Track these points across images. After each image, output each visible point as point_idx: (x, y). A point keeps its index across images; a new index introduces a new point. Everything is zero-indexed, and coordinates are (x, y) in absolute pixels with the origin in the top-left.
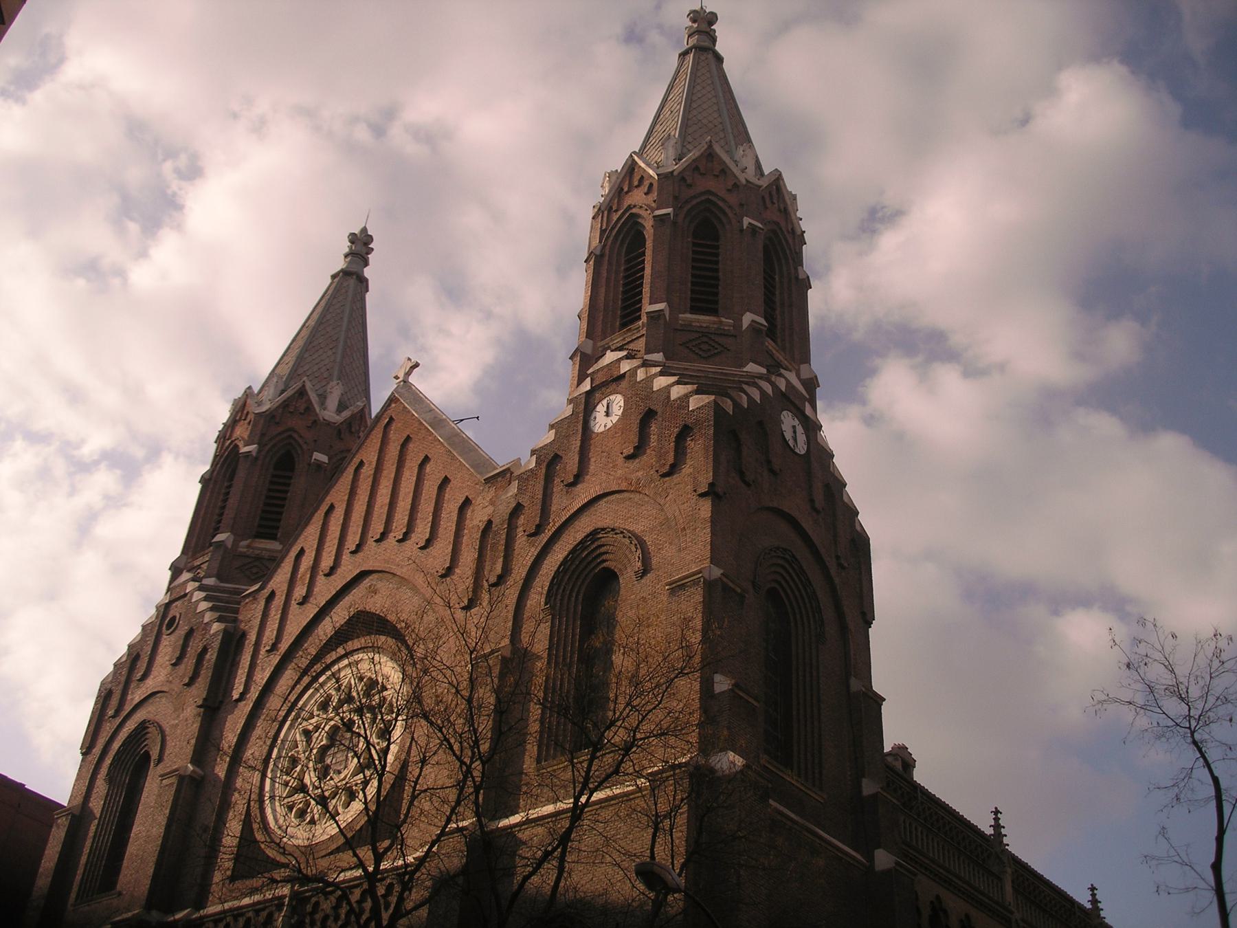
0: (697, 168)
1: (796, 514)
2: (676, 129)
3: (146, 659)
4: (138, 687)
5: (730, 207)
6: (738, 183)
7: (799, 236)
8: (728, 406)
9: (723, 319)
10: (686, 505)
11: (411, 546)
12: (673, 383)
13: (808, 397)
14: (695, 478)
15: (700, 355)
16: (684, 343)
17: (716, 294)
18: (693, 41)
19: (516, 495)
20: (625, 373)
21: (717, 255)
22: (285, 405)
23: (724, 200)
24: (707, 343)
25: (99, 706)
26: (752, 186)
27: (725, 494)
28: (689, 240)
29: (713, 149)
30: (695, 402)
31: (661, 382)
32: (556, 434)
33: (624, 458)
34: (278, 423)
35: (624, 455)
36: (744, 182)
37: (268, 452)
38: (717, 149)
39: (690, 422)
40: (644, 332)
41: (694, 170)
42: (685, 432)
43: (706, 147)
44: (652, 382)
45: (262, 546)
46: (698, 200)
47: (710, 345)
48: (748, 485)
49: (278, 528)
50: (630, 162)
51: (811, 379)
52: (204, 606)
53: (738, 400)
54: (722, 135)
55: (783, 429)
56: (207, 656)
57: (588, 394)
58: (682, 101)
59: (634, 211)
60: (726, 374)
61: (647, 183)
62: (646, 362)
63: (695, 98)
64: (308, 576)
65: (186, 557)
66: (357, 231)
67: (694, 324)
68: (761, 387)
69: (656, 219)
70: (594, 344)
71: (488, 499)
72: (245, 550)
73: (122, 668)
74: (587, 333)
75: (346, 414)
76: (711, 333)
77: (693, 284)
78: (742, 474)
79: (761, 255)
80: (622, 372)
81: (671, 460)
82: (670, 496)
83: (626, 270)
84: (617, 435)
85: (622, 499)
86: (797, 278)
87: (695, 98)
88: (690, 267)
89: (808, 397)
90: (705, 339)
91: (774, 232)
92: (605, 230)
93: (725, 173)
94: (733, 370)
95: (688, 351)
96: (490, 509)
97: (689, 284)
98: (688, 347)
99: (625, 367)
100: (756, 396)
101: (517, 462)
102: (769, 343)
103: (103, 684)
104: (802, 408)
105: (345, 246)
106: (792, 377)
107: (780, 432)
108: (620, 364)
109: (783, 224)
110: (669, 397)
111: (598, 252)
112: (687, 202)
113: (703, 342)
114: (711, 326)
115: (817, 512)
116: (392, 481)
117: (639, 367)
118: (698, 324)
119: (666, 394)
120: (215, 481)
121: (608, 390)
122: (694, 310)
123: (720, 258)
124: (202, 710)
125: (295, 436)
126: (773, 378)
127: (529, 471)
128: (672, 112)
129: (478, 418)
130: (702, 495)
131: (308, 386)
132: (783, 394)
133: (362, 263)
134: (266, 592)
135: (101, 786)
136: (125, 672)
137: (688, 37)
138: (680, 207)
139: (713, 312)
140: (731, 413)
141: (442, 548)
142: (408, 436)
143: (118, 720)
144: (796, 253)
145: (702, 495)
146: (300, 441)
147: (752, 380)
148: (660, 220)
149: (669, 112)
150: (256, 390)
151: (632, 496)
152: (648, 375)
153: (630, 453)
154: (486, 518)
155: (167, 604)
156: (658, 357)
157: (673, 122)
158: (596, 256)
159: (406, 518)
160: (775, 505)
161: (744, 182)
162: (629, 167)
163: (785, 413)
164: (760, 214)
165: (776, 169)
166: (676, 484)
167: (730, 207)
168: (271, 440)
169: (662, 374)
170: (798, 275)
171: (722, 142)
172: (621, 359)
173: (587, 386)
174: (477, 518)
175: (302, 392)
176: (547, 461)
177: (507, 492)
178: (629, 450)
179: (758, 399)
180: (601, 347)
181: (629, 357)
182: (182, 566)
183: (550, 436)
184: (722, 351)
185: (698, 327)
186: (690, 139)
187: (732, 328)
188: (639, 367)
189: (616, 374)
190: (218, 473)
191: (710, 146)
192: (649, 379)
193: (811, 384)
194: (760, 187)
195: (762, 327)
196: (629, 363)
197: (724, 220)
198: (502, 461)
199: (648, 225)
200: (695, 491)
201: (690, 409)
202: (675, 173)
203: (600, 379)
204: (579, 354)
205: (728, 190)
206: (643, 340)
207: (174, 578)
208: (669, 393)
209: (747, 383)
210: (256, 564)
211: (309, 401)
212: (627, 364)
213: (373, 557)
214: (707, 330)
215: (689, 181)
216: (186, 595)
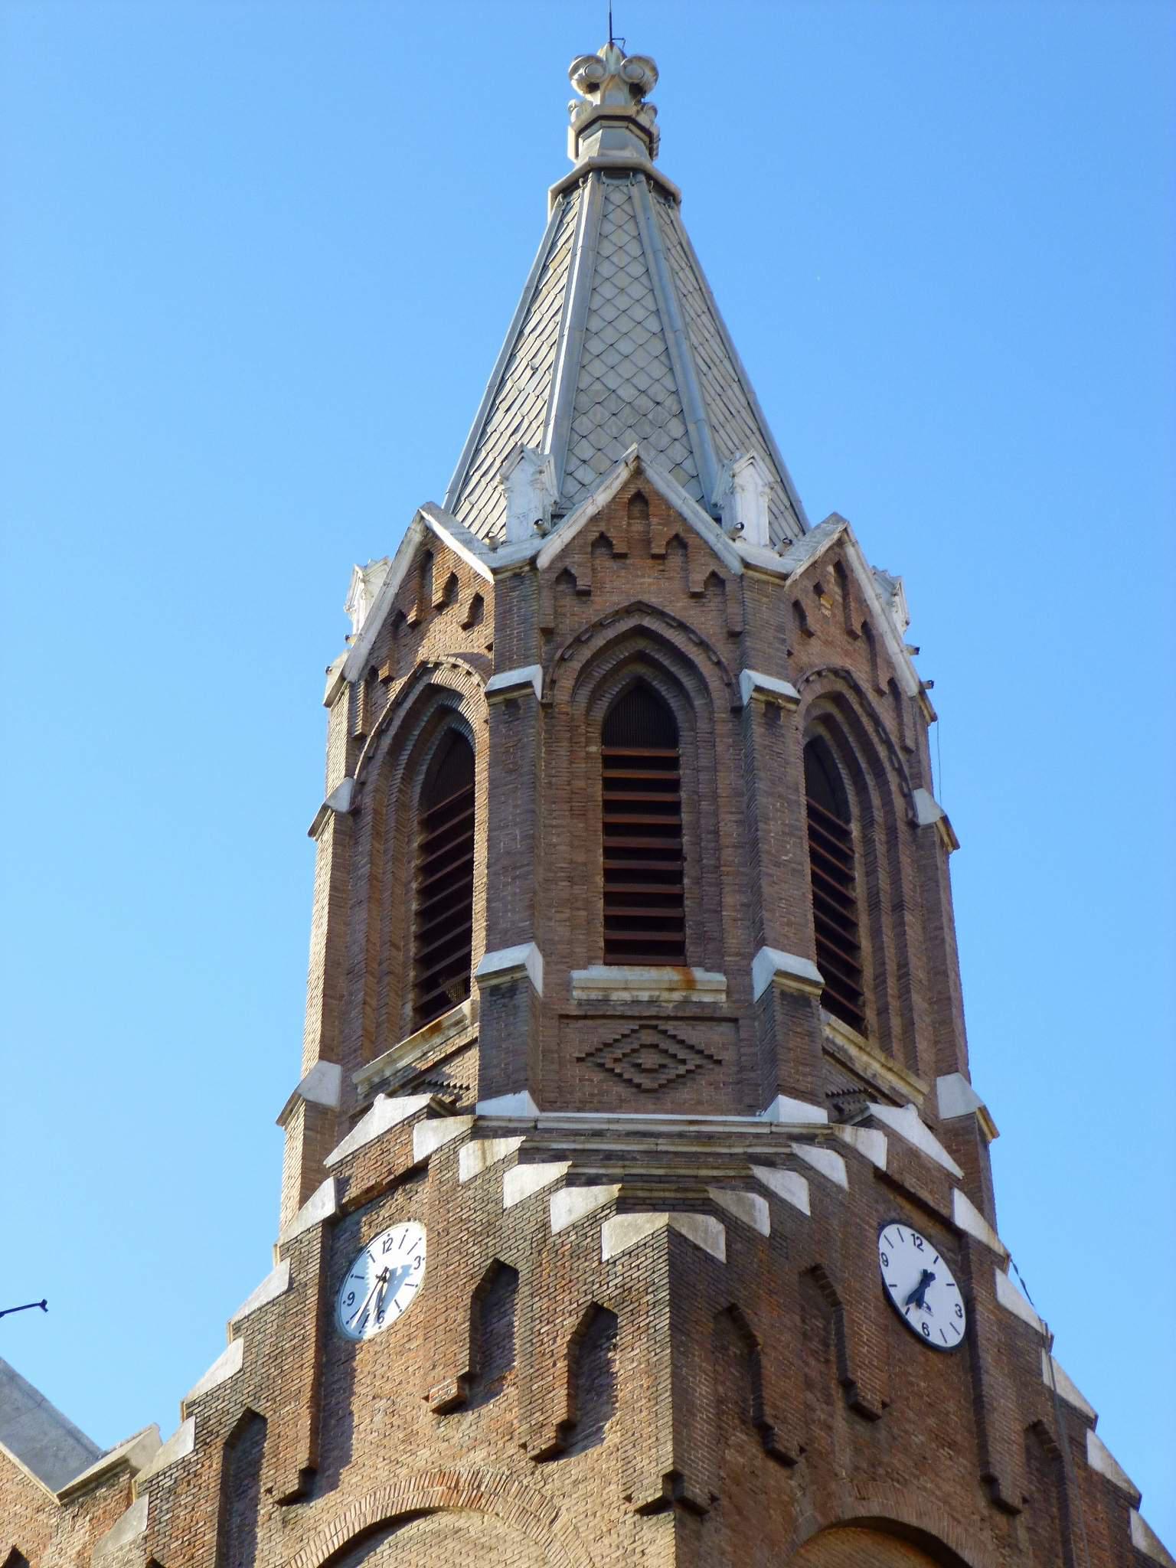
0: (603, 541)
1: (937, 1525)
2: (546, 423)
5: (702, 644)
6: (722, 574)
7: (912, 699)
9: (699, 974)
10: (606, 1541)
12: (558, 1181)
13: (958, 1172)
14: (627, 1461)
15: (638, 1086)
16: (589, 1055)
17: (678, 900)
18: (590, 148)
19: (145, 1538)
20: (428, 1157)
21: (674, 786)
23: (682, 627)
24: (656, 1046)
26: (764, 577)
27: (713, 1499)
28: (593, 749)
29: (648, 481)
32: (247, 1350)
33: (435, 1411)
35: (434, 1404)
36: (737, 567)
38: (662, 480)
39: (607, 1294)
40: (473, 1032)
41: (595, 544)
43: (623, 473)
44: (499, 1181)
46: (610, 633)
47: (666, 1052)
48: (785, 1461)
50: (417, 538)
51: (971, 1116)
53: (745, 1218)
54: (676, 428)
55: (888, 1282)
57: (331, 1225)
58: (561, 336)
59: (438, 678)
60: (710, 1138)
61: (465, 595)
62: (482, 1123)
63: (595, 324)
67: (615, 996)
68: (811, 1168)
69: (494, 700)
70: (345, 1080)
71: (73, 1552)
74: (321, 1042)
76: (668, 1018)
77: (610, 875)
78: (764, 1432)
79: (796, 773)
80: (418, 1156)
81: (559, 1410)
84: (413, 1345)
85: (436, 1534)
86: (913, 825)
87: (595, 324)
88: (600, 826)
89: (958, 1172)
90: (647, 1037)
91: (838, 699)
92: (362, 738)
94: (734, 1122)
95: (602, 1076)
97: (600, 880)
98: (602, 1065)
99: (428, 1139)
100: (796, 1191)
101: (150, 1439)
102: (834, 1030)
104: (944, 1211)
106: (908, 1124)
107: (879, 1292)
108: (411, 1134)
109: (862, 677)
110: (545, 1226)
111: (343, 805)
112: (578, 641)
113: (643, 1046)
114: (665, 995)
115: (1010, 1511)
117: (462, 1140)
118: (626, 996)
119: (540, 1216)
121: (384, 1213)
122: (617, 952)
123: (683, 795)
126: (848, 1134)
127: (176, 1465)
128: (535, 370)
129: (43, 1304)
130: (649, 1510)
132: (881, 1177)
137: (578, 135)
138: (562, 659)
139: (670, 952)
140: (721, 1256)
144: (907, 750)
145: (649, 1510)
149: (529, 372)
151: (461, 1523)
152: (488, 1163)
153: (448, 1398)
156: (518, 1105)
157: (540, 403)
158: (340, 817)
160: (874, 1508)
161: (737, 567)
162: (418, 550)
163: (891, 1231)
164: (790, 654)
165: (835, 514)
166: (576, 1483)
167: (702, 644)
169: (526, 1155)
170: (915, 815)
171: (678, 452)
173: (324, 1202)
176: (225, 1432)
177: (120, 1532)
178: (448, 1389)
179: (764, 1226)
180: (362, 1082)
183: (229, 1360)
184: (698, 1067)
185: (625, 1003)
186: (585, 450)
187: (723, 997)
188: (462, 1140)
189: (401, 1165)
191: (638, 472)
192: (492, 1173)
194: (784, 577)
195: (808, 989)
196: (435, 1130)
197: (688, 683)
199: (476, 713)
200: (629, 1499)
201: (605, 1257)
202: (543, 562)
204: (302, 1109)
205: (695, 596)
206: (474, 1054)
208: (546, 1210)
209: (769, 1162)
212: (430, 1134)
214: (653, 1011)
215: (581, 584)
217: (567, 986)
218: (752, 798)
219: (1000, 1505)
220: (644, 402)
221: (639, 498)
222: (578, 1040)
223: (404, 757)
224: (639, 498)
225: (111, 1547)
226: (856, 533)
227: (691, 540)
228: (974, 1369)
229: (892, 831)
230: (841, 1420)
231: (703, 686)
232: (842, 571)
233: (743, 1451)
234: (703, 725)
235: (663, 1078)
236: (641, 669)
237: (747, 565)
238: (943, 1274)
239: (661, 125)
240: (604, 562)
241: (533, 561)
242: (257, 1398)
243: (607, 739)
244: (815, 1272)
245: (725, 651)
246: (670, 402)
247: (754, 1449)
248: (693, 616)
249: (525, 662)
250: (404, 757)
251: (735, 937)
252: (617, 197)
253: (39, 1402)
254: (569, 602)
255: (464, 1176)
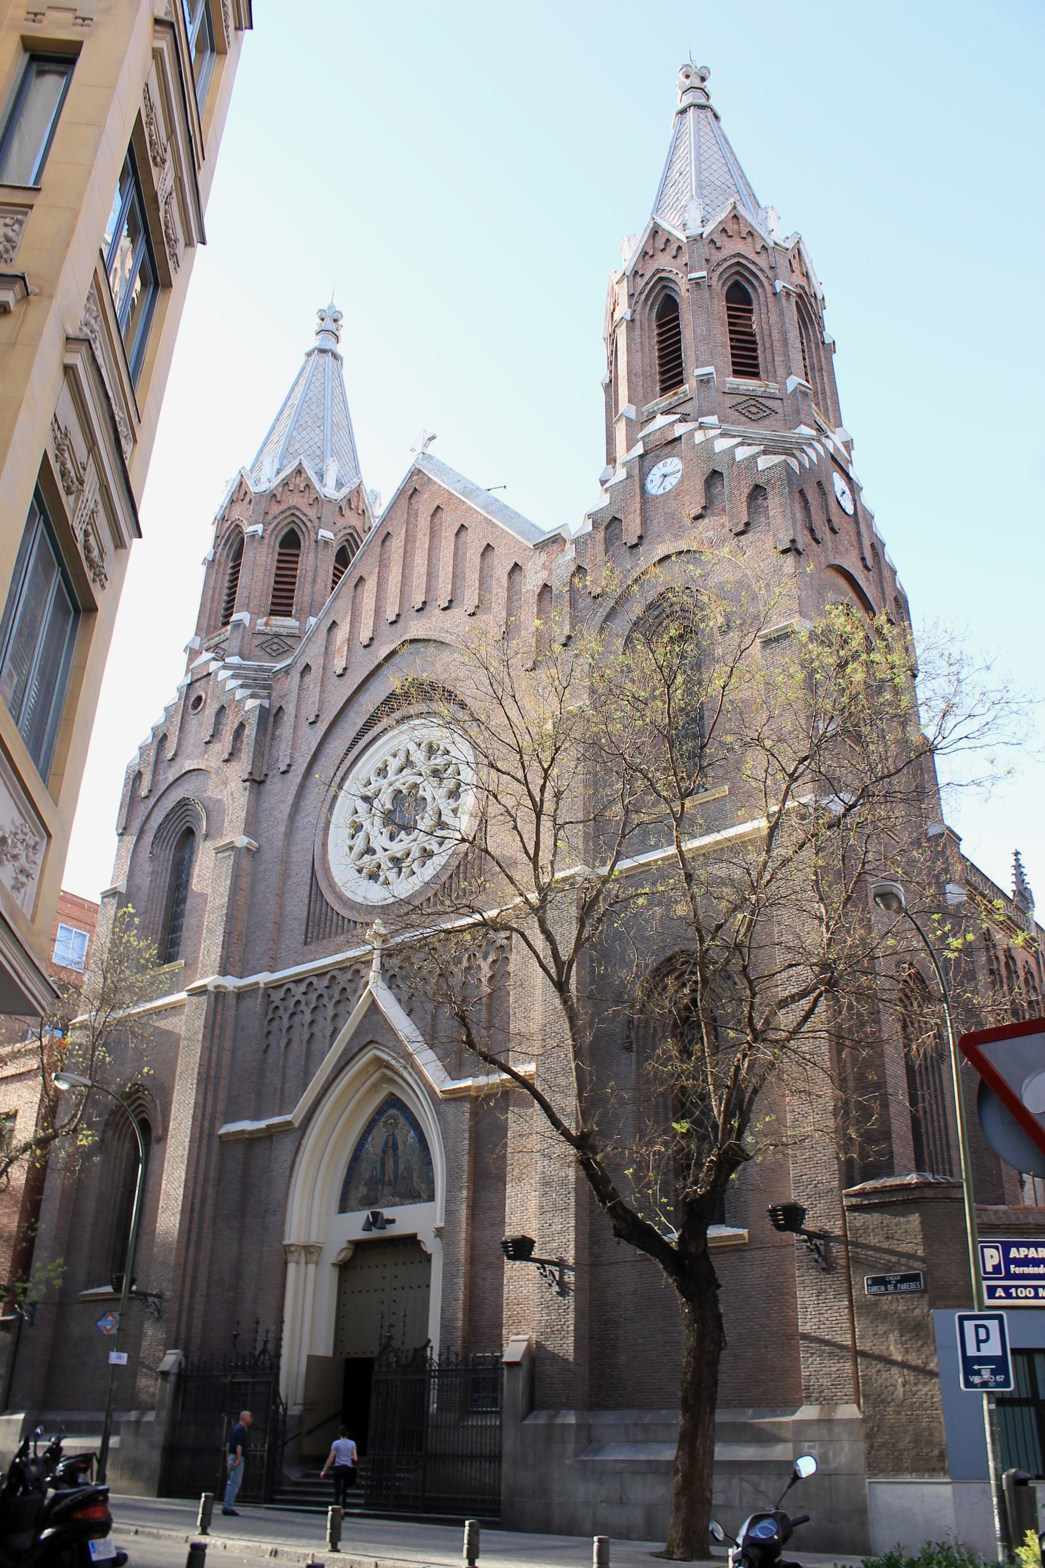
0: (724, 230)
3: (175, 740)
4: (170, 766)
5: (761, 270)
8: (794, 464)
11: (458, 613)
22: (285, 483)
23: (754, 263)
25: (130, 787)
30: (764, 462)
31: (722, 445)
32: (611, 498)
34: (279, 502)
36: (772, 245)
37: (274, 529)
38: (742, 210)
39: (761, 482)
42: (758, 492)
43: (730, 208)
45: (279, 623)
46: (729, 263)
48: (818, 542)
49: (291, 605)
50: (651, 226)
52: (232, 684)
56: (247, 732)
63: (703, 159)
64: (346, 648)
65: (199, 638)
66: (325, 308)
72: (263, 628)
73: (149, 750)
75: (345, 491)
80: (677, 435)
82: (748, 553)
83: (659, 335)
86: (823, 343)
90: (753, 402)
92: (633, 295)
93: (752, 235)
96: (544, 574)
99: (680, 429)
103: (129, 767)
105: (315, 324)
110: (734, 459)
115: (868, 569)
116: (427, 552)
120: (219, 562)
122: (736, 373)
124: (248, 784)
125: (298, 513)
130: (784, 552)
131: (306, 464)
133: (333, 339)
134: (300, 667)
135: (147, 867)
136: (153, 753)
139: (756, 375)
141: (493, 620)
142: (438, 507)
143: (152, 801)
145: (784, 552)
146: (304, 518)
147: (809, 442)
148: (697, 283)
150: (248, 468)
154: (541, 583)
155: (189, 685)
159: (450, 587)
160: (837, 562)
167: (761, 270)
168: (275, 518)
172: (674, 422)
173: (639, 449)
174: (532, 581)
175: (299, 471)
176: (605, 524)
178: (697, 510)
181: (684, 419)
182: (197, 647)
190: (221, 555)
191: (735, 208)
192: (710, 442)
193: (848, 445)
198: (548, 526)
202: (704, 236)
203: (654, 441)
205: (758, 253)
207: (191, 660)
208: (733, 453)
209: (805, 444)
210: (276, 640)
211: (308, 479)
213: (417, 629)
215: (718, 245)
216: (209, 674)
217: (724, 383)
218: (783, 324)
219: (866, 567)
220: (723, 186)
221: (735, 216)
222: (730, 401)
223: (649, 303)
224: (735, 216)
225: (560, 561)
226: (803, 239)
227: (755, 233)
228: (857, 523)
229: (817, 344)
230: (828, 531)
231: (762, 286)
232: (798, 250)
233: (808, 538)
234: (762, 299)
235: (759, 416)
236: (738, 277)
237: (776, 244)
238: (848, 492)
239: (341, 334)
240: (724, 237)
241: (701, 235)
242: (617, 513)
243: (728, 301)
244: (819, 483)
245: (770, 274)
246: (733, 187)
247: (809, 537)
248: (756, 259)
249: (701, 270)
250: (649, 303)
251: (781, 371)
252: (701, 116)
253: (519, 516)
254: (714, 251)
255: (697, 442)
